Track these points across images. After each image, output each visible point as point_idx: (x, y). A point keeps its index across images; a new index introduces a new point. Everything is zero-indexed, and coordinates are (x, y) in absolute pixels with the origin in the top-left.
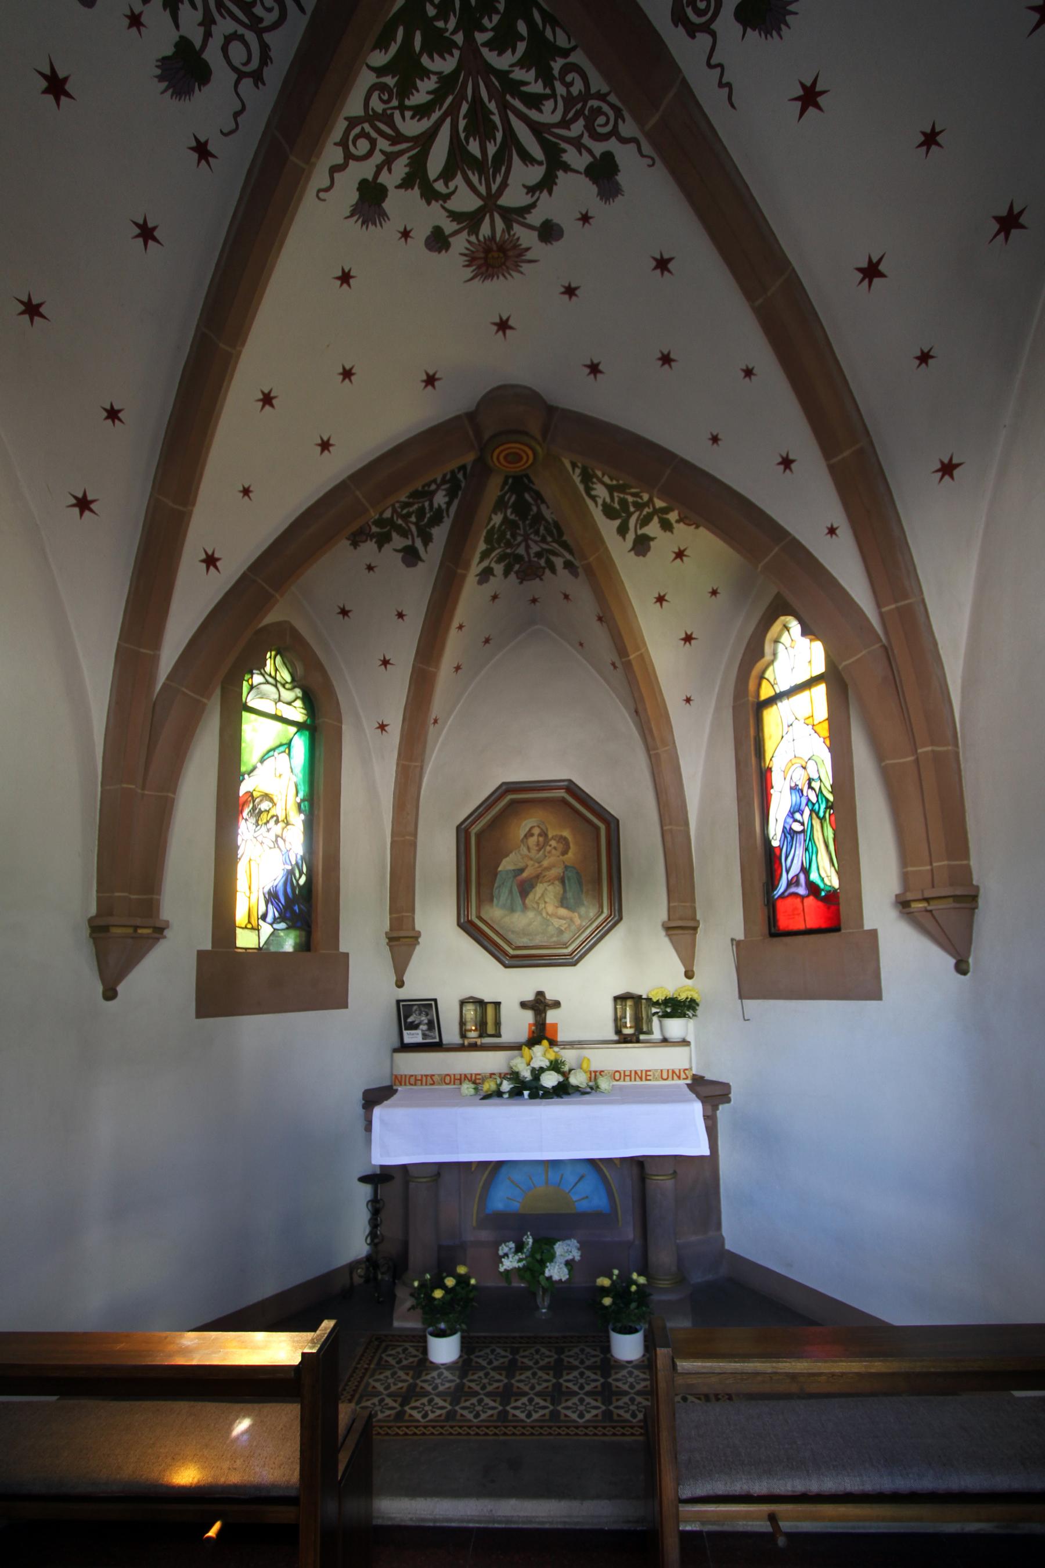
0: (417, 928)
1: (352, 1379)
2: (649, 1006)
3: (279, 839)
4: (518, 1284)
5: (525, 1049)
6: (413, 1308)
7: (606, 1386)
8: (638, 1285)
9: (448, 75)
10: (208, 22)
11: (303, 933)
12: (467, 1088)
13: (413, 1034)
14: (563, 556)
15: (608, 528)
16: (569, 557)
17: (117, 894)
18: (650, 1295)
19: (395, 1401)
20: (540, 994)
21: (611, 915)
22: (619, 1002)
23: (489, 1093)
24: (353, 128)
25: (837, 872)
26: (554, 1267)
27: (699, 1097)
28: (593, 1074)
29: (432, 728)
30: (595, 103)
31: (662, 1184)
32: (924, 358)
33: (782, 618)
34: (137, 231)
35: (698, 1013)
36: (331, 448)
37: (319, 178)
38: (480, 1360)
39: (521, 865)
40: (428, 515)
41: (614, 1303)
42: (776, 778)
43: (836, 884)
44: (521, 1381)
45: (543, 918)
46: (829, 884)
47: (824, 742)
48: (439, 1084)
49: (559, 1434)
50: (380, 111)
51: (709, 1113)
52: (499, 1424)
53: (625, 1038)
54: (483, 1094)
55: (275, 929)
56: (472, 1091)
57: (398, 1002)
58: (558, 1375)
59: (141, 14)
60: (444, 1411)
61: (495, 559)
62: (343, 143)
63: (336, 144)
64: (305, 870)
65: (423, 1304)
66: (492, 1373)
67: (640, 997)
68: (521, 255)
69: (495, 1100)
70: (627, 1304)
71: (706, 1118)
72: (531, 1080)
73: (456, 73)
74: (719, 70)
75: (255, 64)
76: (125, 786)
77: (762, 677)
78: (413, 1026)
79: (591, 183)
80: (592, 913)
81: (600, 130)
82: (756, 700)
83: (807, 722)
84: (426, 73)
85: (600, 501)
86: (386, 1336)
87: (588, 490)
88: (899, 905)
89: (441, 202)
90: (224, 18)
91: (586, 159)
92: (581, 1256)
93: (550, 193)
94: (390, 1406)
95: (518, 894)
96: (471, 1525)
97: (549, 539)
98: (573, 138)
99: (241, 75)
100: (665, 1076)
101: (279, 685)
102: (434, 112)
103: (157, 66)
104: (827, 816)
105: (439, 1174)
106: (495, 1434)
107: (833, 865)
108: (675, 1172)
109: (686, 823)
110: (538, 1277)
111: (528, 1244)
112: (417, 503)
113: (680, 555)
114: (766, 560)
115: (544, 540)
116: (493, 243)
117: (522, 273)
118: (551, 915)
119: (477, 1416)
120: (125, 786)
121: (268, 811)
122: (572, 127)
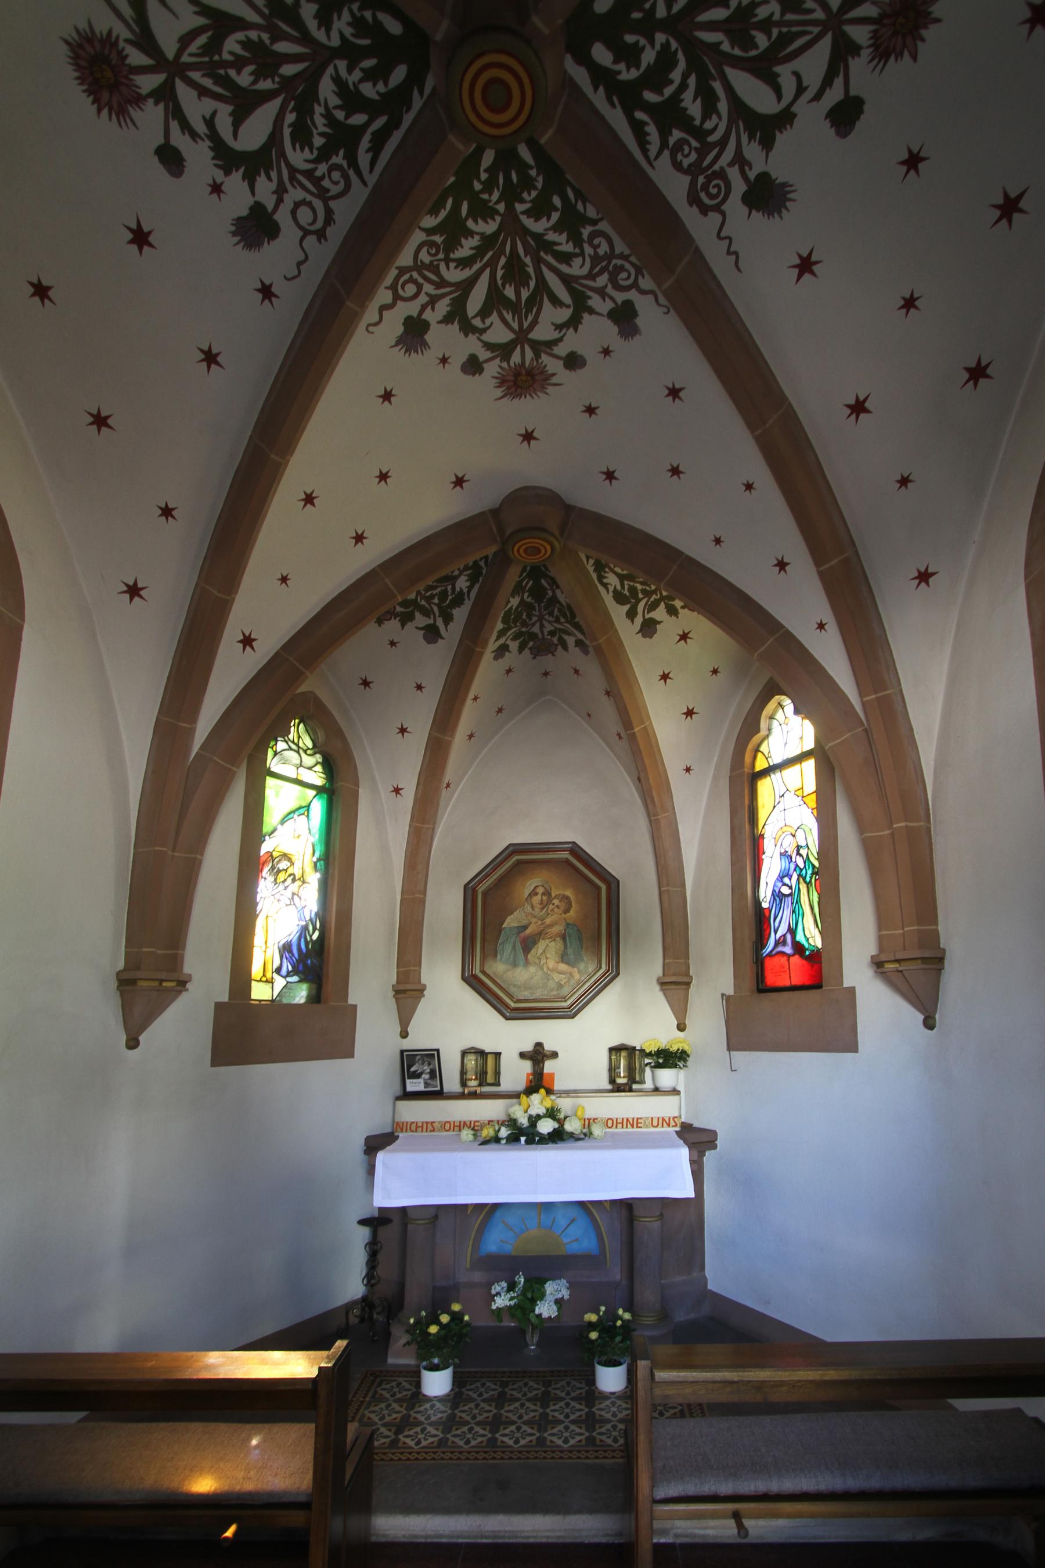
0: (423, 981)
1: (359, 1392)
2: (642, 1057)
3: (295, 897)
4: (509, 1323)
5: (523, 1098)
6: (408, 1343)
7: (590, 1415)
8: (623, 1321)
9: (490, 235)
10: (280, 191)
11: (314, 986)
12: (467, 1135)
13: (415, 1083)
14: (574, 635)
15: (618, 612)
16: (580, 637)
17: (144, 950)
18: (634, 1330)
19: (390, 1430)
20: (539, 1045)
21: (609, 970)
22: (614, 1053)
23: (487, 1139)
24: (403, 275)
25: (820, 933)
26: (545, 1305)
27: (686, 1142)
28: (587, 1122)
29: (444, 793)
30: (619, 262)
31: (649, 1225)
32: (904, 481)
33: (777, 697)
34: (202, 356)
35: (688, 1064)
36: (364, 541)
37: (371, 314)
38: (471, 1393)
39: (525, 922)
40: (450, 598)
41: (600, 1337)
42: (768, 845)
43: (820, 946)
44: (509, 1411)
45: (544, 972)
46: (813, 944)
47: (812, 813)
48: (439, 1131)
49: (545, 1458)
50: (427, 262)
51: (695, 1158)
52: (489, 1449)
53: (618, 1088)
54: (481, 1140)
55: (288, 982)
56: (471, 1137)
57: (402, 1052)
58: (545, 1405)
59: (222, 183)
60: (436, 1439)
61: (511, 637)
62: (393, 287)
63: (386, 288)
64: (318, 926)
65: (419, 1339)
66: (482, 1405)
67: (634, 1048)
68: (547, 379)
69: (493, 1146)
70: (612, 1338)
71: (692, 1162)
72: (527, 1127)
73: (496, 234)
74: (728, 241)
75: (319, 224)
76: (156, 848)
77: (757, 750)
78: (416, 1075)
79: (612, 324)
80: (591, 968)
81: (622, 283)
82: (751, 772)
83: (797, 793)
84: (471, 233)
85: (611, 588)
86: (381, 1372)
87: (600, 578)
88: (875, 965)
89: (477, 335)
90: (296, 188)
91: (609, 305)
92: (570, 1295)
93: (576, 330)
94: (396, 1410)
95: (521, 950)
96: (460, 1540)
97: (562, 620)
98: (599, 288)
99: (306, 233)
100: (655, 1123)
101: (301, 751)
102: (476, 263)
103: (232, 224)
104: (813, 880)
105: (436, 1217)
106: (485, 1458)
107: (818, 927)
108: (661, 1214)
109: (683, 885)
110: (529, 1315)
111: (520, 1283)
112: (441, 586)
113: (684, 637)
114: (762, 649)
115: (557, 620)
116: (523, 369)
117: (547, 394)
118: (551, 971)
119: (468, 1442)
120: (156, 848)
121: (286, 870)
122: (598, 279)
